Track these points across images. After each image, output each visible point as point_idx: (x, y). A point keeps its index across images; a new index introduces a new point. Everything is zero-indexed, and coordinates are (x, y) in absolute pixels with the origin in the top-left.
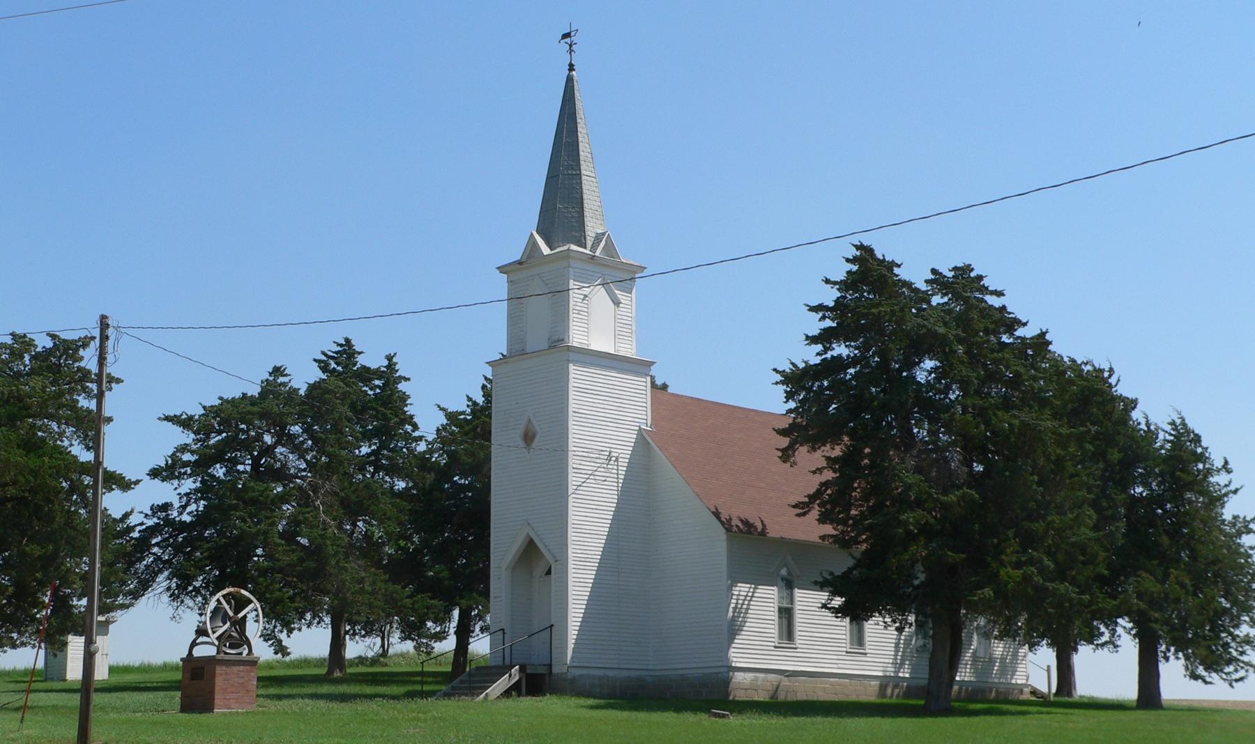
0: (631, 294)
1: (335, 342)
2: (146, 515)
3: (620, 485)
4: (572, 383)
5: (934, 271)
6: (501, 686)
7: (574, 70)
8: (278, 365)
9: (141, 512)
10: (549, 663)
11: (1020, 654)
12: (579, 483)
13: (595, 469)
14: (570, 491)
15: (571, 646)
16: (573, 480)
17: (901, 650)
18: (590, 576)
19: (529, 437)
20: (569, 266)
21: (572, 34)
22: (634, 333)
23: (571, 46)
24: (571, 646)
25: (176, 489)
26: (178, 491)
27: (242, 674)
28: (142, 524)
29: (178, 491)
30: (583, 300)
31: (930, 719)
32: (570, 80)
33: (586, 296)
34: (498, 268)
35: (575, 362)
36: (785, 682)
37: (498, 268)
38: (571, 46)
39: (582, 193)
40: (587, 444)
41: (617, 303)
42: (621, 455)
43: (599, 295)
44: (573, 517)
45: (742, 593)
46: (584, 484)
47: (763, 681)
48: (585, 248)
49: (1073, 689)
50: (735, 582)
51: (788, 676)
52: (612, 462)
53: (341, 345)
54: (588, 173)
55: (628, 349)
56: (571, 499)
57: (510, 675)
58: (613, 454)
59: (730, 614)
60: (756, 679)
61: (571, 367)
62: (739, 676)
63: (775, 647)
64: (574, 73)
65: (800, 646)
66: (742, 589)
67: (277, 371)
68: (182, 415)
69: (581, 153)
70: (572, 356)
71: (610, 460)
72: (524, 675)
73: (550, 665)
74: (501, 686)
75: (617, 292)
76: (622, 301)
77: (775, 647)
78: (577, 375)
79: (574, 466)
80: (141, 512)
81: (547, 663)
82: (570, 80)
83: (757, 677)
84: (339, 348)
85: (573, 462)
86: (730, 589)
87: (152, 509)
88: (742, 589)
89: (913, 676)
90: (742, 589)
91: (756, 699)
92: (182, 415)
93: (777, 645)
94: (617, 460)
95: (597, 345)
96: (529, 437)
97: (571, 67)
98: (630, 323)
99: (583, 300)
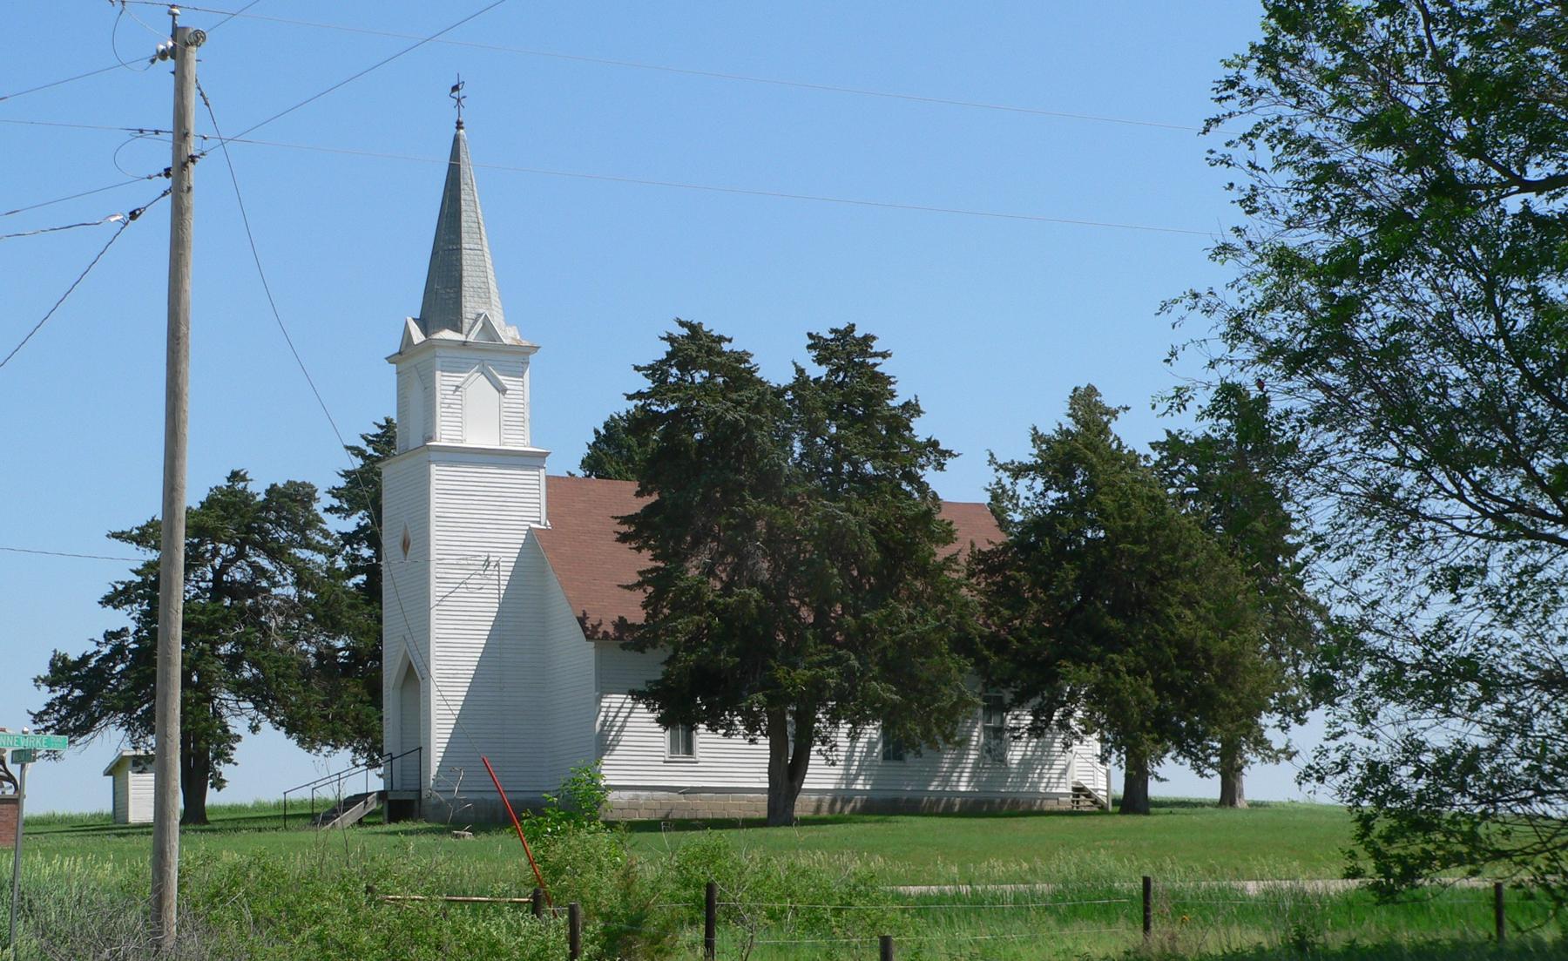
0: (522, 377)
1: (375, 423)
2: (98, 643)
3: (502, 592)
4: (434, 485)
5: (810, 335)
6: (354, 814)
7: (462, 128)
8: (236, 469)
9: (92, 640)
10: (418, 787)
11: (842, 763)
12: (445, 594)
13: (467, 576)
14: (433, 603)
15: (434, 770)
16: (436, 590)
17: (857, 763)
18: (460, 693)
19: (406, 545)
20: (435, 356)
21: (460, 86)
22: (527, 421)
23: (459, 100)
24: (434, 770)
25: (129, 614)
26: (132, 616)
27: (5, 813)
28: (98, 652)
29: (132, 616)
30: (455, 391)
31: (647, 834)
32: (456, 140)
33: (458, 387)
34: (387, 359)
35: (438, 463)
36: (682, 799)
37: (387, 359)
38: (459, 100)
39: (461, 270)
40: (460, 551)
41: (502, 390)
42: (503, 559)
43: (477, 385)
44: (437, 631)
45: (613, 705)
46: (453, 594)
47: (648, 799)
48: (461, 333)
49: (1237, 795)
50: (604, 689)
51: (683, 793)
52: (491, 568)
53: (381, 427)
54: (472, 246)
55: (519, 442)
56: (433, 612)
57: (366, 803)
58: (491, 559)
59: (598, 728)
60: (637, 797)
61: (433, 468)
62: (612, 796)
63: (665, 762)
64: (461, 131)
65: (701, 759)
66: (614, 701)
67: (235, 476)
68: (132, 531)
69: (464, 224)
70: (433, 456)
71: (488, 566)
72: (386, 804)
73: (420, 791)
74: (354, 814)
75: (500, 377)
76: (508, 387)
77: (665, 762)
78: (440, 476)
79: (438, 575)
80: (92, 640)
81: (412, 787)
82: (456, 140)
83: (638, 796)
84: (379, 431)
85: (435, 570)
86: (599, 700)
87: (105, 636)
88: (613, 700)
89: (876, 787)
90: (613, 700)
91: (637, 818)
92: (132, 531)
93: (667, 759)
94: (497, 565)
95: (473, 441)
96: (406, 545)
97: (459, 125)
98: (522, 410)
99: (455, 391)
